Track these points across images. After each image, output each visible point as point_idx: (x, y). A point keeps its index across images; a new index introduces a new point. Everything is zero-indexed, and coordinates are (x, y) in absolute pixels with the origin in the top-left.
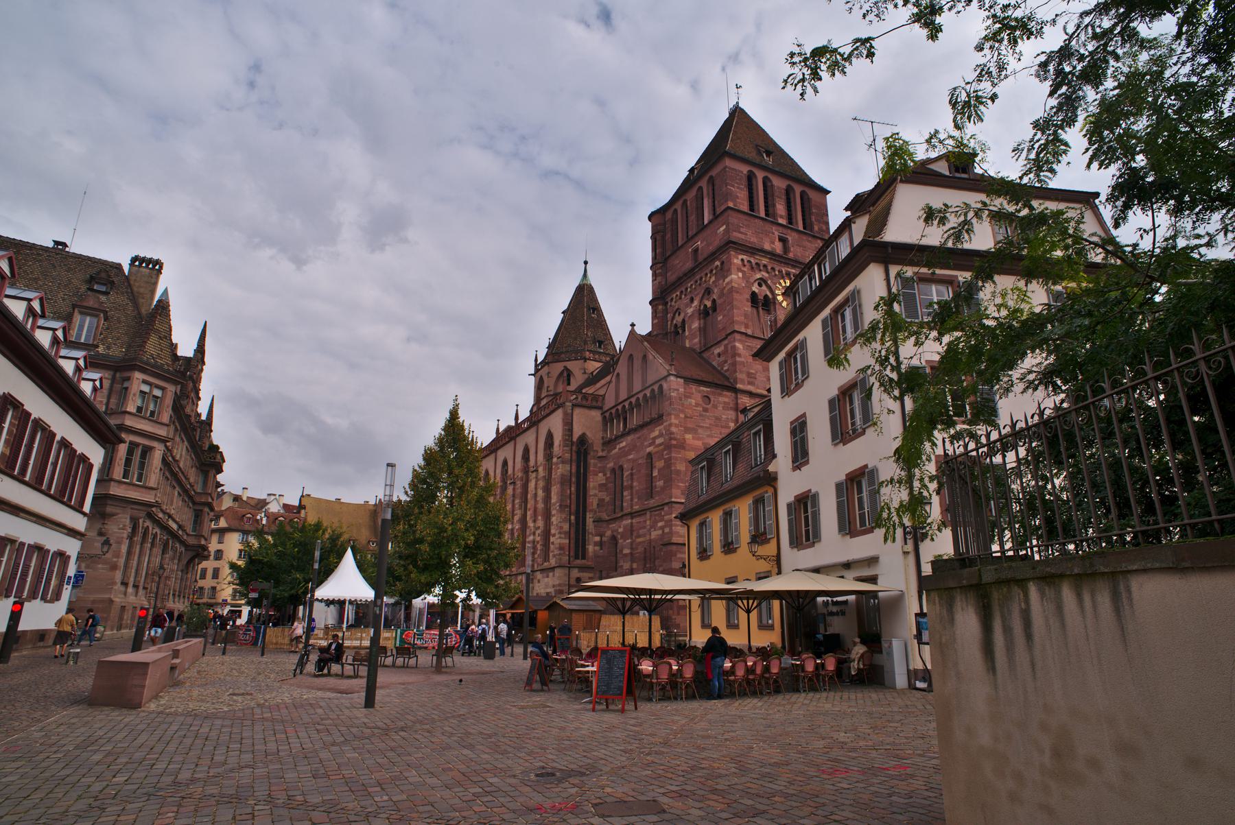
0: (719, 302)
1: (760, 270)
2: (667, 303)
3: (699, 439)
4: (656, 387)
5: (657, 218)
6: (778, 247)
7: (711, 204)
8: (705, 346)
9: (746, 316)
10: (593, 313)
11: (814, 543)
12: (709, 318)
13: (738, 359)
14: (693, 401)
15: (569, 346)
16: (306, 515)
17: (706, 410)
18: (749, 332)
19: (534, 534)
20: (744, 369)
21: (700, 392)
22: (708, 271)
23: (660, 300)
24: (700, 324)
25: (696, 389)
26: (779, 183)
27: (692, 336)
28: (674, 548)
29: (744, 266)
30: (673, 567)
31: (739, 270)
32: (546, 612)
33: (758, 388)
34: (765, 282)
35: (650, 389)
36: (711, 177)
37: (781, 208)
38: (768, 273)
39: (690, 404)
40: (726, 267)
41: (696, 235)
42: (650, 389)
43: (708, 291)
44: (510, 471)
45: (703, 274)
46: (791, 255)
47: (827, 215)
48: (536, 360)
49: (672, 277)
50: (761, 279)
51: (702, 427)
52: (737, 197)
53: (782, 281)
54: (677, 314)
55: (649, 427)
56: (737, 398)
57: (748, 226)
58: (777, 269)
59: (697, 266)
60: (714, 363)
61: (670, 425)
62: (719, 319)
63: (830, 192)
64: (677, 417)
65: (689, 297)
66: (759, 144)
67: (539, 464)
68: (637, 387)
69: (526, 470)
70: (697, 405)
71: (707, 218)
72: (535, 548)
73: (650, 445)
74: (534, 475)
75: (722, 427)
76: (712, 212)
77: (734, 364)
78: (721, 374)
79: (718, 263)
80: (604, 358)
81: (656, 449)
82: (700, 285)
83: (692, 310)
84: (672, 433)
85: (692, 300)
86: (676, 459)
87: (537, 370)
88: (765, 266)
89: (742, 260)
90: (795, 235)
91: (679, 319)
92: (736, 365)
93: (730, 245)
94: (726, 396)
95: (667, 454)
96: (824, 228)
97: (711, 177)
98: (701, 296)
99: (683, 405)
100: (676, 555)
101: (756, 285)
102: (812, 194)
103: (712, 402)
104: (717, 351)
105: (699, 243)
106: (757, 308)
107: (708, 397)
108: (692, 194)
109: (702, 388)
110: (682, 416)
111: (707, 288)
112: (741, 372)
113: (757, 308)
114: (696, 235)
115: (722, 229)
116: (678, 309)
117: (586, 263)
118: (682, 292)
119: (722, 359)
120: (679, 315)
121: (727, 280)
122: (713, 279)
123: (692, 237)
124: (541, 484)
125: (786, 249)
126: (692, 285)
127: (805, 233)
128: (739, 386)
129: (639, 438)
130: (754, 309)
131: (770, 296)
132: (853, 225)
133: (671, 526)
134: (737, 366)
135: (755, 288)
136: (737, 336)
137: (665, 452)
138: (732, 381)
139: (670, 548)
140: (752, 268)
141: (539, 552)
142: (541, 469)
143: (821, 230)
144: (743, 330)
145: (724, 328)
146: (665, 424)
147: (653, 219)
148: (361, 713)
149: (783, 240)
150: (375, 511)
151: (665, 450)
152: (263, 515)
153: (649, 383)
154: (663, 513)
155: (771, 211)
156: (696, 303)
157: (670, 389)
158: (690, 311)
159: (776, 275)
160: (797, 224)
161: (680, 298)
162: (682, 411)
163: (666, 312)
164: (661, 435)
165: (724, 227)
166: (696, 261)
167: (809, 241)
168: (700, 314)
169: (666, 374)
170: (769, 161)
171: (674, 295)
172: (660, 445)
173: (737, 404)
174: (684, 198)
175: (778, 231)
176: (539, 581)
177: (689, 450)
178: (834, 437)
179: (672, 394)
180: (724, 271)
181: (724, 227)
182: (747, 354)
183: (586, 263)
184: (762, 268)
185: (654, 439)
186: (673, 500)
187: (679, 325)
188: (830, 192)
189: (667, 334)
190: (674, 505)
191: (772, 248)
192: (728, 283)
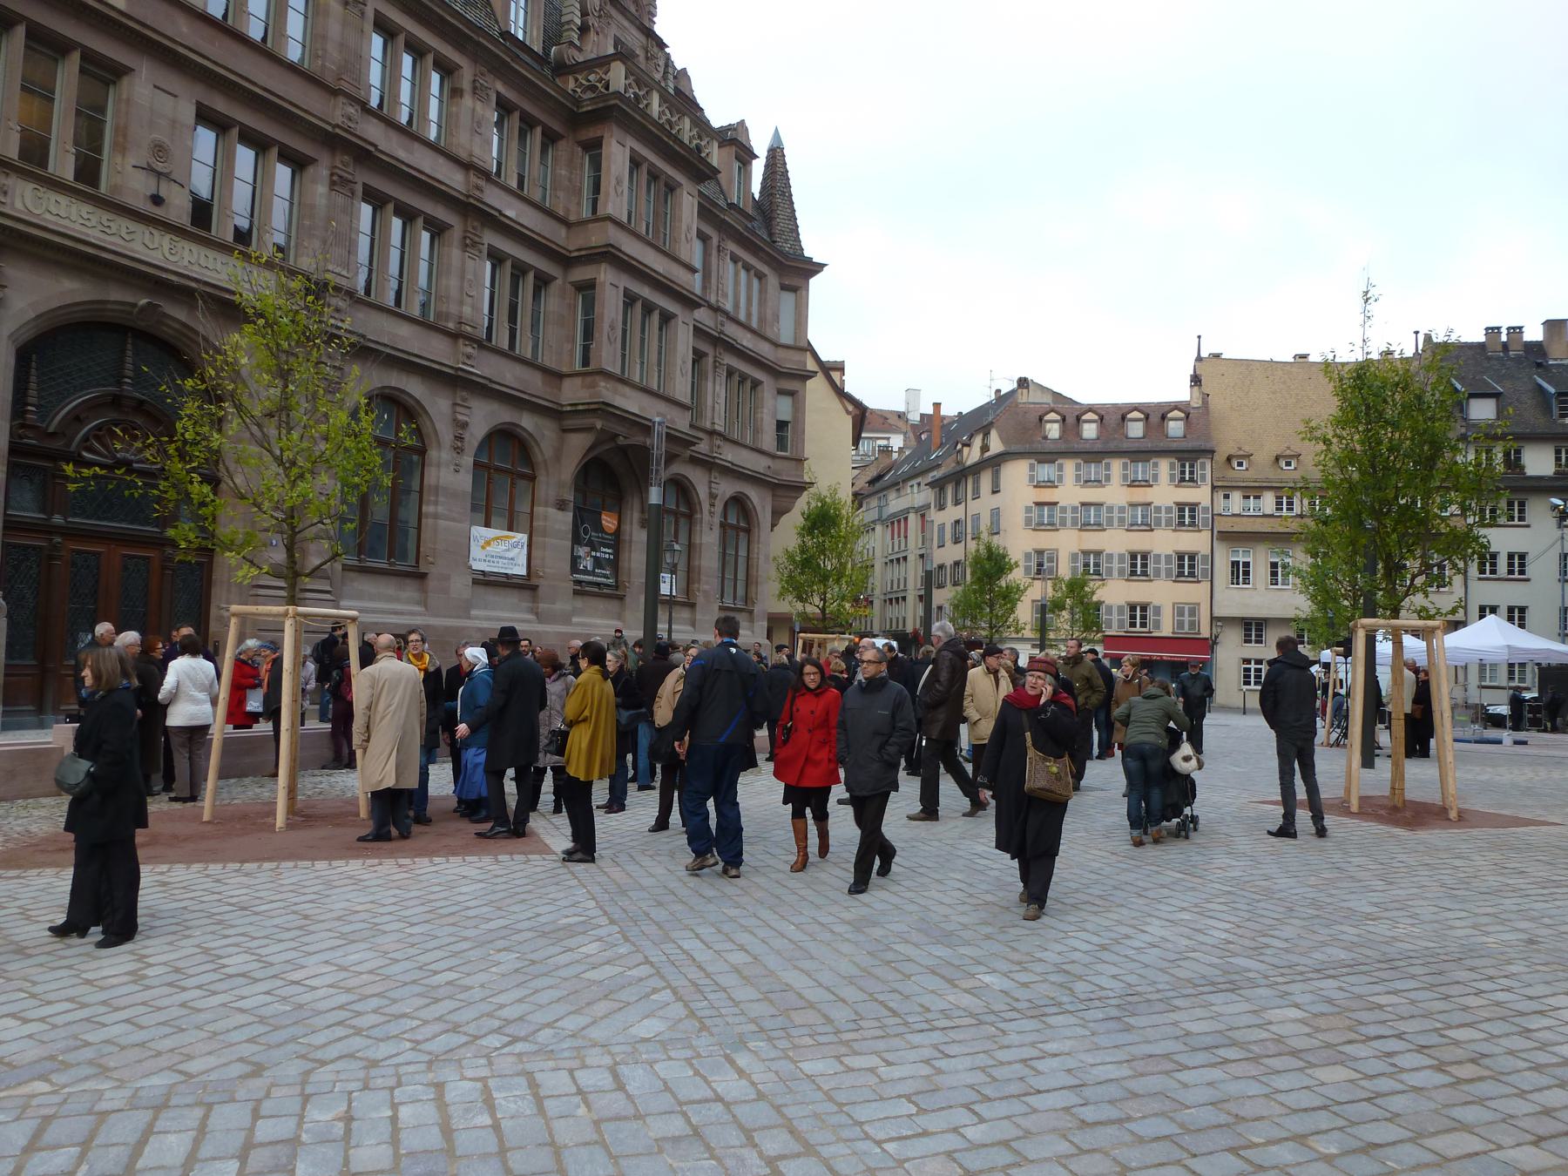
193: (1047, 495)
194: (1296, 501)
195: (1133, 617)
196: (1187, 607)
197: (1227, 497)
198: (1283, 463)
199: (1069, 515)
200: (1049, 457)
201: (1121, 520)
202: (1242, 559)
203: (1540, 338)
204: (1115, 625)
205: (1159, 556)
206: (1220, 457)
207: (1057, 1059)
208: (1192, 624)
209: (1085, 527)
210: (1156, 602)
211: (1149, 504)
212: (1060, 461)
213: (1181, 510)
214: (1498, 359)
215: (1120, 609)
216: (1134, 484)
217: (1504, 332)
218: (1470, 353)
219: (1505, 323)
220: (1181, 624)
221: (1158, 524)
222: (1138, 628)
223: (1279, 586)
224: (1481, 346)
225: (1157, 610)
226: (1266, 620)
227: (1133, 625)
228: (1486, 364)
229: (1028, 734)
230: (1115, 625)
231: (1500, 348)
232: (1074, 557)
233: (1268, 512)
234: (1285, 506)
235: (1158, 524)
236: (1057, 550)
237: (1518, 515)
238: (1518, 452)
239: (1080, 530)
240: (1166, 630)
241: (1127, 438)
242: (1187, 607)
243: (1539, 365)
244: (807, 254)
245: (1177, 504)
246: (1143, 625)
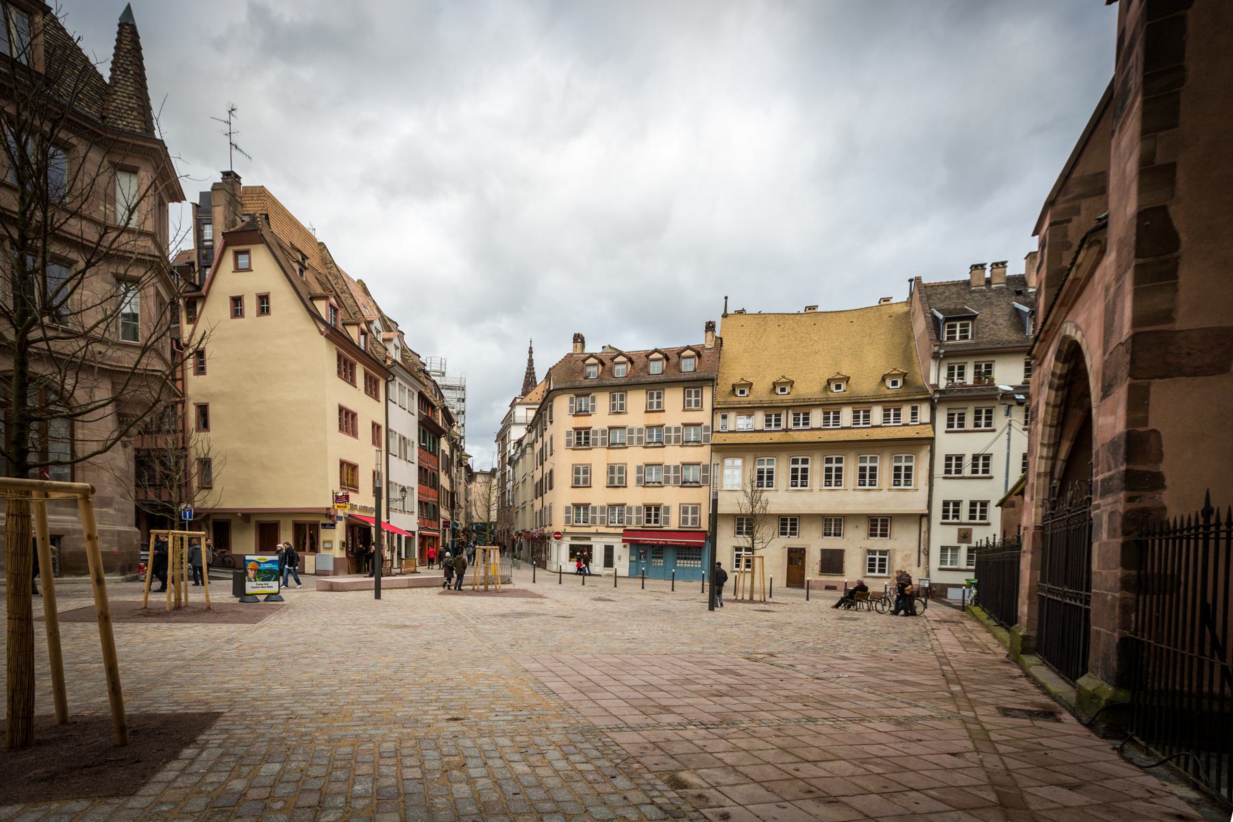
193: (582, 422)
194: (783, 418)
195: (649, 515)
196: (690, 507)
197: (724, 417)
198: (778, 390)
199: (599, 437)
200: (584, 391)
201: (640, 440)
202: (765, 467)
204: (634, 521)
205: (669, 467)
206: (724, 386)
208: (694, 520)
209: (612, 446)
210: (666, 504)
211: (662, 426)
212: (593, 394)
214: (981, 291)
215: (638, 509)
216: (578, 414)
217: (988, 268)
218: (954, 289)
220: (685, 520)
221: (669, 441)
222: (653, 524)
223: (867, 487)
225: (667, 510)
226: (800, 516)
227: (649, 521)
228: (968, 297)
230: (634, 521)
231: (983, 283)
233: (759, 428)
234: (773, 423)
235: (669, 441)
236: (591, 465)
237: (985, 421)
238: (989, 366)
239: (608, 448)
240: (674, 524)
241: (649, 374)
242: (690, 507)
243: (1019, 293)
245: (575, 429)
246: (656, 521)
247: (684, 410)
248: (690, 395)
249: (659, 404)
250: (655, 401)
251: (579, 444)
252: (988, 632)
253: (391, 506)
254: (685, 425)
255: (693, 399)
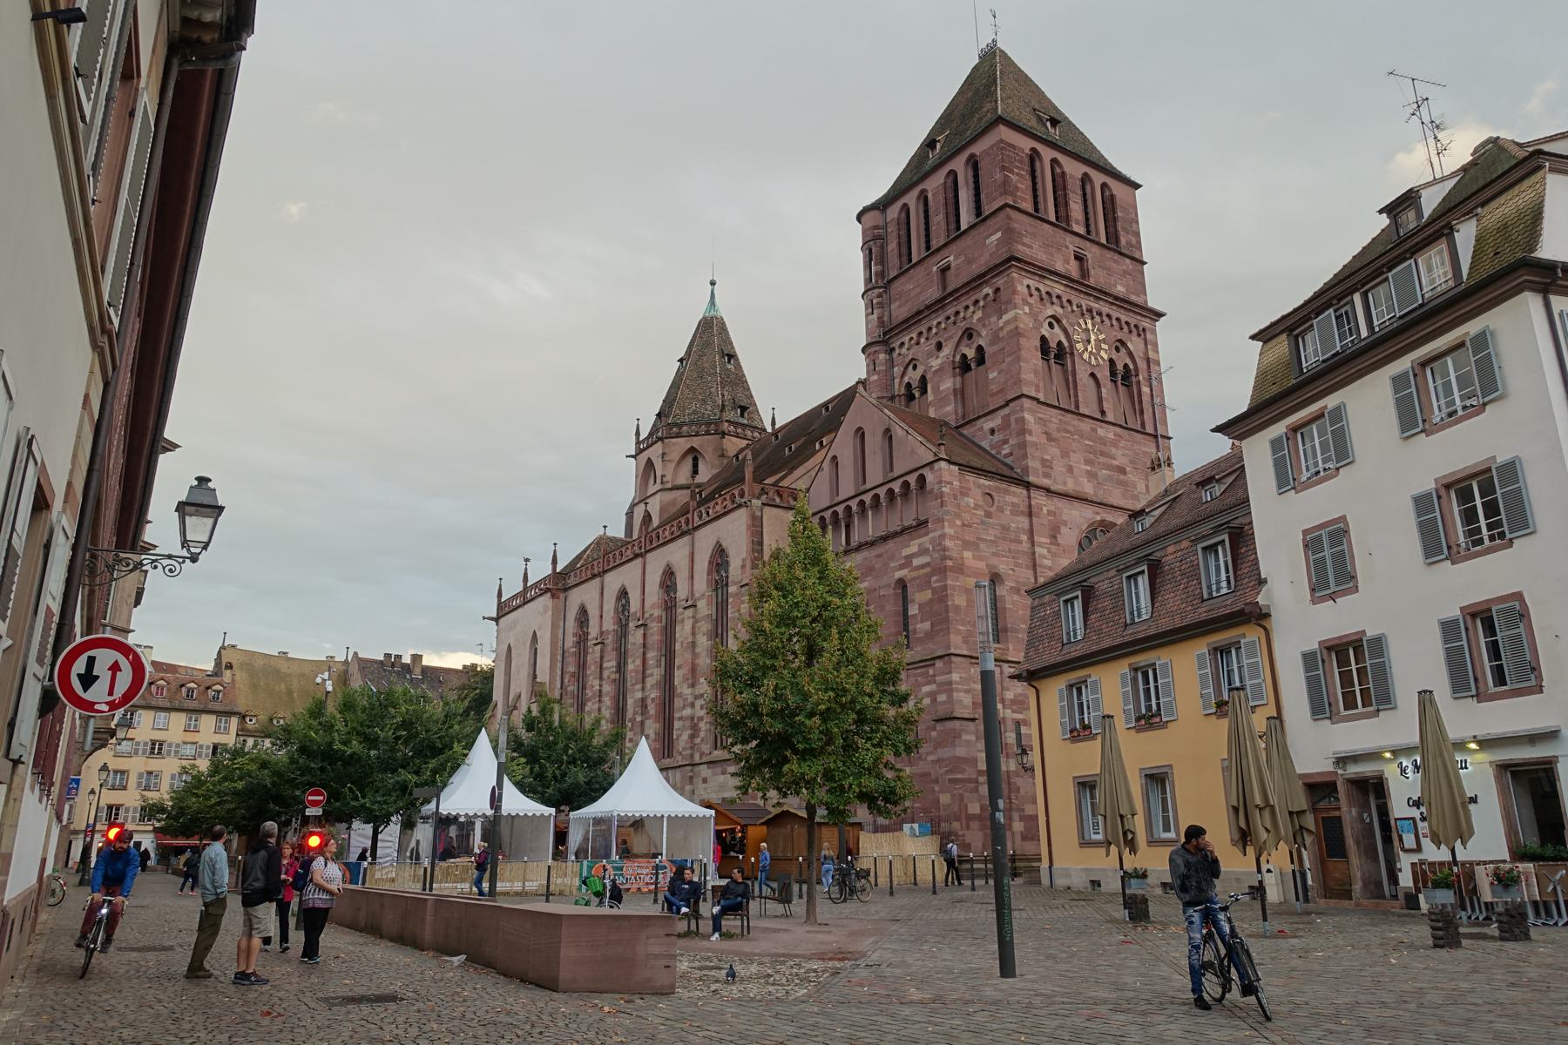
0: (988, 350)
1: (1052, 303)
2: (893, 349)
3: (980, 558)
4: (912, 479)
5: (870, 218)
6: (1073, 269)
7: (972, 199)
8: (964, 417)
9: (1036, 372)
10: (729, 362)
11: (1378, 710)
12: (970, 376)
13: (1028, 438)
14: (972, 500)
15: (695, 412)
16: (233, 680)
17: (988, 515)
18: (1041, 397)
19: (693, 705)
20: (1037, 454)
21: (979, 486)
22: (970, 302)
23: (882, 340)
24: (954, 384)
25: (974, 482)
26: (1073, 169)
27: (942, 402)
28: (957, 724)
29: (1031, 295)
30: (958, 755)
31: (1026, 302)
32: (764, 828)
33: (1056, 482)
34: (1058, 321)
35: (900, 481)
36: (972, 156)
37: (1076, 208)
38: (1063, 307)
39: (968, 505)
40: (1003, 296)
41: (945, 245)
42: (900, 481)
43: (969, 334)
44: (634, 606)
45: (960, 308)
46: (1092, 282)
47: (1137, 222)
48: (638, 434)
49: (900, 311)
50: (1052, 317)
51: (986, 540)
52: (1017, 188)
53: (1081, 321)
54: (911, 367)
55: (897, 540)
56: (1029, 497)
57: (1033, 235)
58: (1075, 303)
59: (944, 298)
60: (984, 444)
61: (943, 536)
62: (991, 376)
63: (1140, 186)
64: (952, 525)
65: (933, 341)
66: (1037, 107)
67: (697, 595)
68: (875, 475)
69: (670, 606)
70: (977, 507)
71: (966, 219)
72: (695, 729)
73: (902, 567)
74: (690, 612)
75: (1011, 541)
76: (973, 212)
77: (1023, 445)
78: (999, 460)
79: (988, 290)
80: (749, 433)
81: (914, 574)
82: (954, 323)
83: (939, 361)
84: (945, 549)
85: (939, 346)
86: (953, 588)
87: (639, 451)
88: (1059, 297)
89: (1028, 286)
90: (1095, 249)
91: (913, 376)
92: (1026, 446)
93: (1011, 261)
94: (1014, 494)
95: (937, 581)
96: (1134, 241)
97: (972, 156)
98: (956, 339)
99: (958, 506)
100: (960, 737)
101: (1046, 325)
102: (1117, 188)
103: (996, 504)
104: (988, 424)
105: (951, 258)
106: (1048, 360)
107: (990, 495)
108: (934, 184)
109: (982, 481)
110: (958, 522)
111: (967, 329)
112: (1034, 458)
113: (1048, 360)
114: (945, 245)
115: (994, 238)
116: (913, 359)
117: (713, 283)
118: (920, 334)
119: (997, 437)
120: (915, 367)
121: (1005, 317)
122: (979, 314)
123: (938, 250)
124: (705, 626)
125: (1084, 273)
126: (939, 323)
127: (1110, 249)
128: (1031, 479)
129: (879, 556)
130: (1045, 362)
131: (1066, 344)
132: (1456, 234)
133: (950, 692)
134: (1028, 449)
135: (1045, 331)
136: (1026, 403)
137: (935, 578)
138: (1019, 471)
139: (949, 724)
140: (1042, 299)
141: (702, 734)
142: (702, 604)
143: (1129, 244)
144: (1033, 394)
145: (1001, 391)
146: (931, 535)
147: (863, 219)
148: (996, 986)
149: (1079, 258)
150: (346, 672)
151: (933, 573)
152: (326, 676)
153: (897, 472)
154: (931, 672)
155: (1062, 213)
156: (947, 351)
157: (940, 482)
158: (935, 363)
159: (1073, 311)
160: (1097, 233)
161: (918, 343)
162: (958, 516)
163: (891, 363)
164: (923, 551)
165: (999, 234)
166: (944, 288)
167: (1115, 261)
168: (954, 368)
169: (932, 458)
170: (1054, 133)
171: (907, 338)
172: (922, 567)
173: (1030, 506)
174: (920, 187)
175: (1072, 243)
176: (705, 781)
177: (968, 576)
178: (1427, 555)
179: (944, 489)
180: (999, 302)
181: (999, 234)
182: (1040, 431)
183: (713, 283)
184: (1054, 299)
185: (909, 558)
186: (952, 651)
187: (915, 384)
188: (1140, 186)
189: (892, 398)
190: (954, 659)
191: (1067, 269)
192: (1008, 322)
203: (409, 662)
207: (343, 992)
213: (154, 744)
219: (394, 653)
224: (382, 662)
229: (92, 866)
232: (141, 775)
244: (162, 457)
247: (215, 732)
248: (220, 722)
249: (195, 726)
250: (193, 723)
251: (152, 753)
252: (980, 57)
253: (670, 771)
254: (185, 743)
255: (223, 725)
